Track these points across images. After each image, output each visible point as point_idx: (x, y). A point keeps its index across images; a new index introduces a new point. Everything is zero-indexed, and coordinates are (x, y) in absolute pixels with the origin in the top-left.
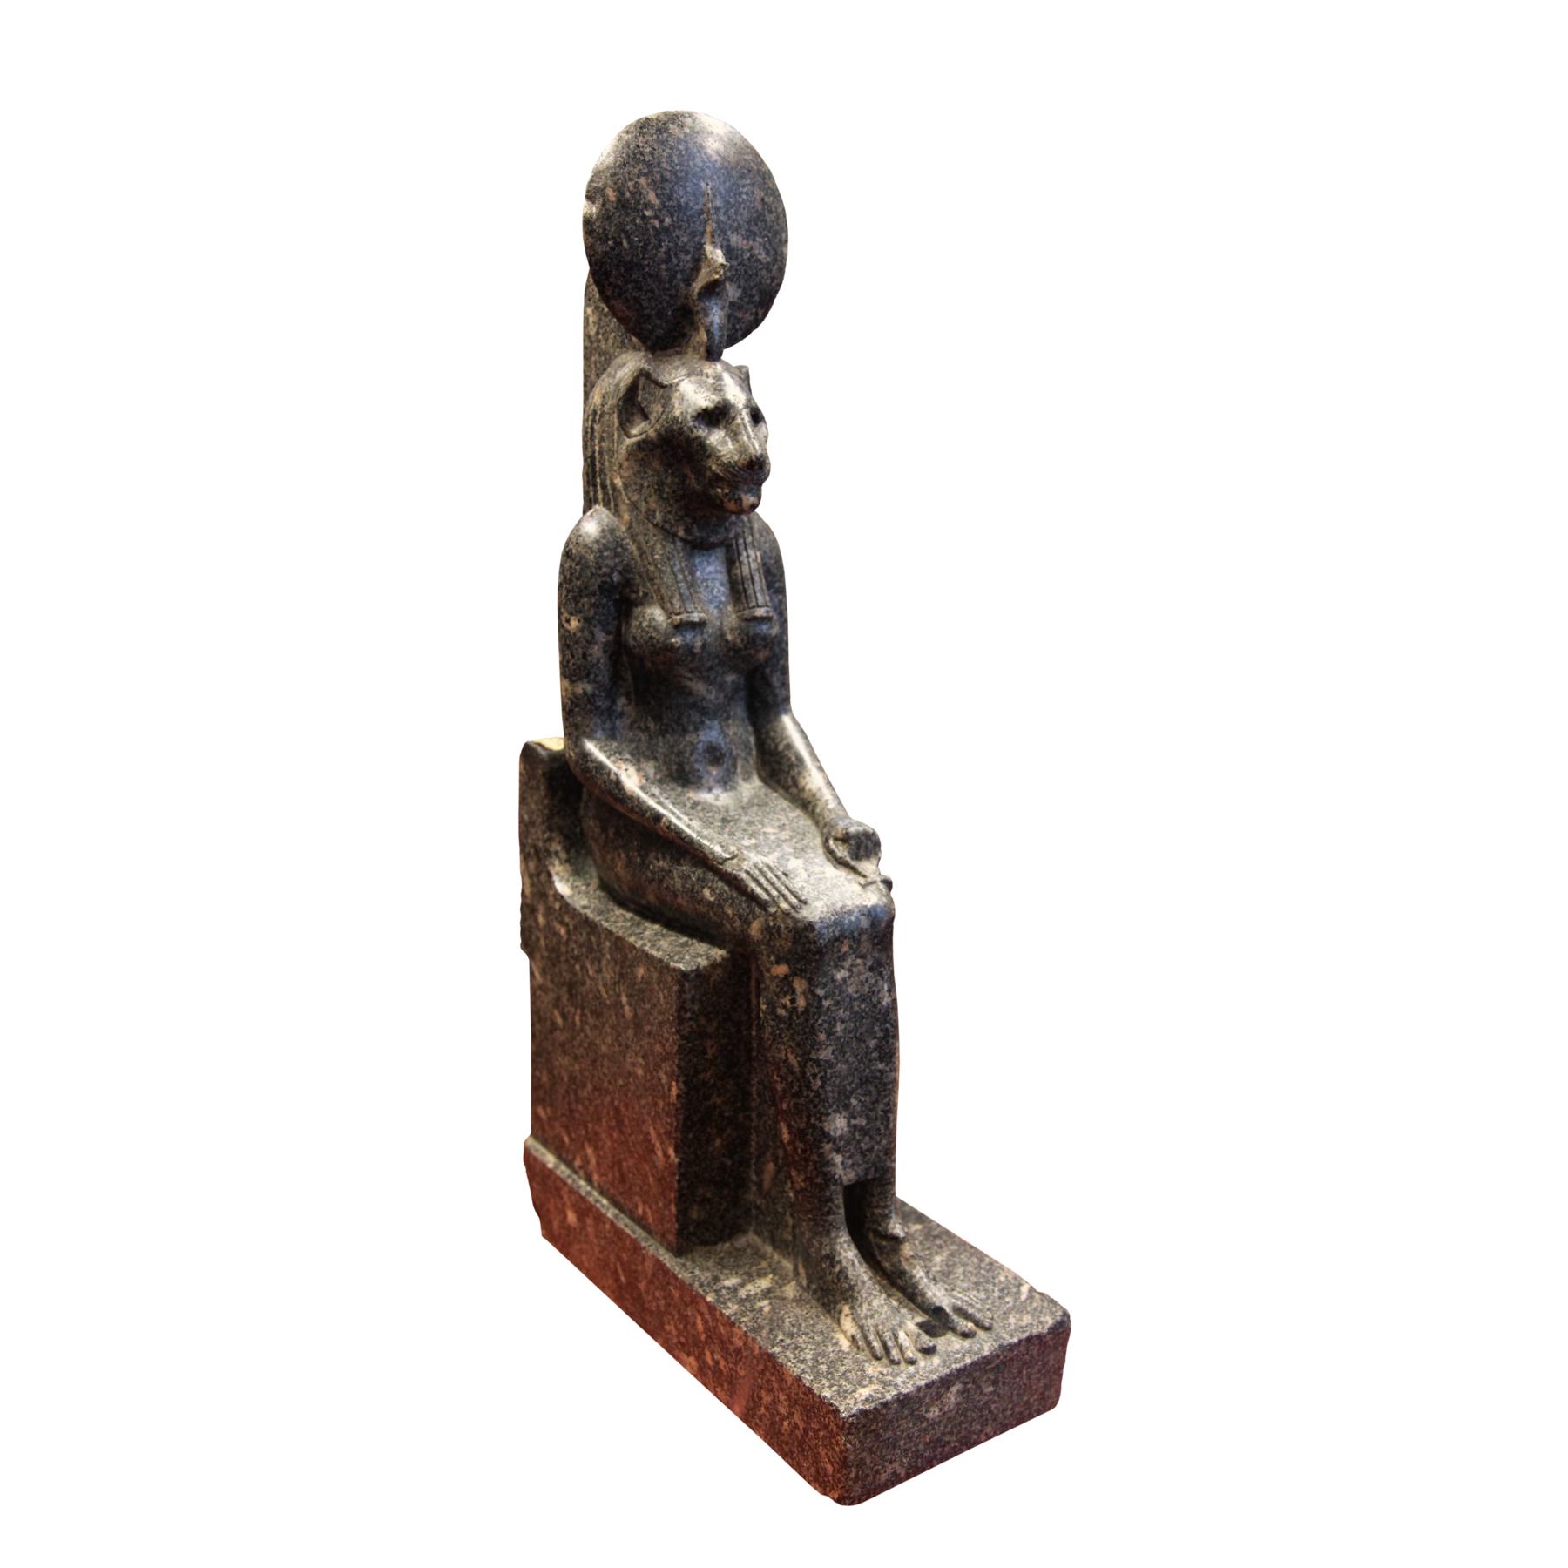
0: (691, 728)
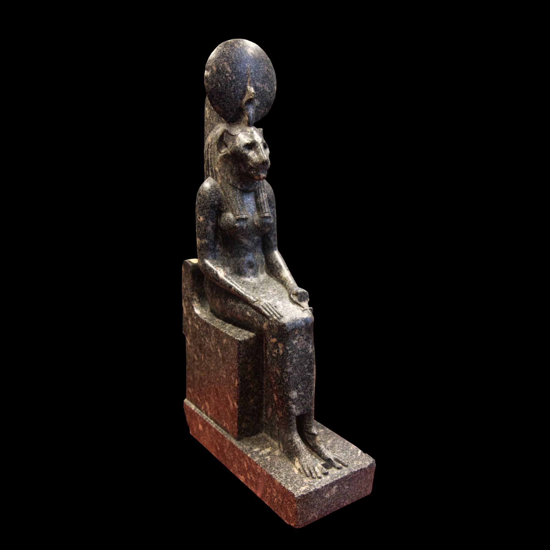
0: (242, 255)
